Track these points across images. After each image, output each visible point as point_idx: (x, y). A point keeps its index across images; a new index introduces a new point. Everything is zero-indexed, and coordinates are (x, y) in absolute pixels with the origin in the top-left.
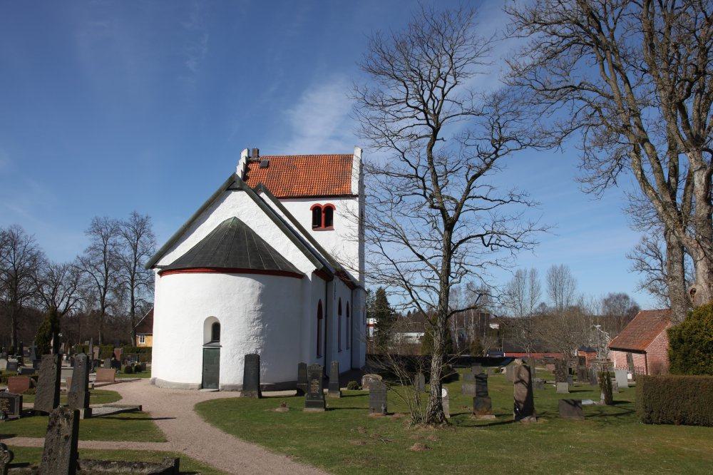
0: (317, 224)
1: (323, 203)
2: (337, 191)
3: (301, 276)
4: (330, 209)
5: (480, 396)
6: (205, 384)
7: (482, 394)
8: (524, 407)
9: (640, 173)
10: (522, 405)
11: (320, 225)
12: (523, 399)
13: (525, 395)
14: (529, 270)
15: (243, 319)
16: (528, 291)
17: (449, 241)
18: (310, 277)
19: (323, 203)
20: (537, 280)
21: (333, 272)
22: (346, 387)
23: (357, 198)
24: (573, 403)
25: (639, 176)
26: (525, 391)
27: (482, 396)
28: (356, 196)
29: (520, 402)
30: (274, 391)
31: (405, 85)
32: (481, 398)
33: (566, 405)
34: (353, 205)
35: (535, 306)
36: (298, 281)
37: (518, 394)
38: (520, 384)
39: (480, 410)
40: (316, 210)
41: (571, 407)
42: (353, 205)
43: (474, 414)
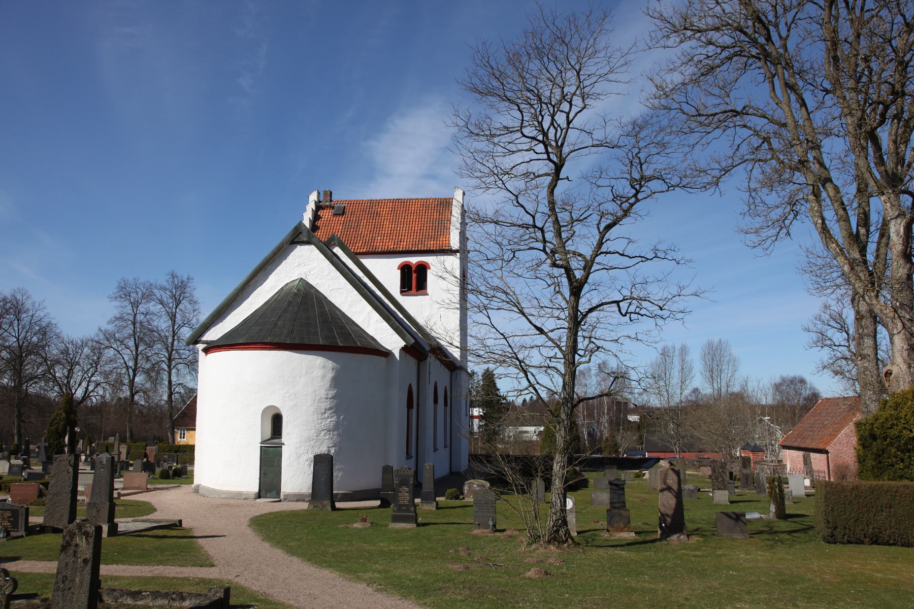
1: (414, 260)
2: (432, 245)
3: (387, 354)
4: (422, 269)
5: (615, 508)
8: (672, 521)
9: (820, 221)
10: (669, 520)
11: (410, 289)
12: (670, 512)
14: (678, 346)
18: (397, 355)
19: (414, 260)
20: (688, 358)
21: (427, 348)
23: (458, 254)
24: (734, 516)
25: (819, 226)
26: (673, 502)
27: (618, 508)
29: (668, 516)
32: (617, 510)
34: (453, 262)
35: (687, 392)
36: (382, 359)
37: (664, 505)
38: (666, 493)
40: (405, 270)
41: (732, 522)
42: (453, 262)
43: (608, 531)
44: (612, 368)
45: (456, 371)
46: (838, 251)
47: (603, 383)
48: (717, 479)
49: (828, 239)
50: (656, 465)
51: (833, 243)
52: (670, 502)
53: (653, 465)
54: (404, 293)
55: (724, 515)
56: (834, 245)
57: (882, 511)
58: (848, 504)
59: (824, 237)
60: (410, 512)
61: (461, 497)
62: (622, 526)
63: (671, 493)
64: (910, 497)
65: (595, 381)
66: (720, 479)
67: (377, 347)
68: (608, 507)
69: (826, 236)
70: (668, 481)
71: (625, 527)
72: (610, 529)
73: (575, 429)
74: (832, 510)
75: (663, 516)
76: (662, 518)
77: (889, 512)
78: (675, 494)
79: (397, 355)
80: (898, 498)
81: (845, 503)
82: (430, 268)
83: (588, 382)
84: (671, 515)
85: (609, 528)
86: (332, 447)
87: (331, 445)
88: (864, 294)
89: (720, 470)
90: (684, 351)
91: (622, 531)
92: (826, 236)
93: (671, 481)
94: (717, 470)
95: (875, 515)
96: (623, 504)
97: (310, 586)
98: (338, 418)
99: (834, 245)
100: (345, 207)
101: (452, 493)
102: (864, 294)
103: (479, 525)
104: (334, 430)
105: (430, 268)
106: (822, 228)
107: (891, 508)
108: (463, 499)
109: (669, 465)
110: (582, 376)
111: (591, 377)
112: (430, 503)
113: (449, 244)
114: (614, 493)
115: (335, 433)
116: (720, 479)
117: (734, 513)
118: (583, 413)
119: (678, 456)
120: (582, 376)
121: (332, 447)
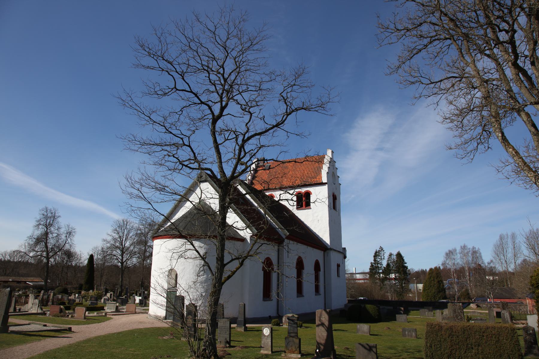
0: (300, 206)
1: (303, 190)
4: (308, 194)
5: (291, 337)
6: (168, 316)
7: (293, 335)
8: (324, 348)
9: (500, 135)
10: (322, 347)
11: (302, 206)
12: (323, 342)
13: (325, 337)
14: (509, 234)
15: (192, 271)
16: (510, 250)
17: (289, 200)
18: (249, 241)
19: (303, 190)
20: (517, 241)
21: (284, 237)
22: (270, 323)
23: (327, 185)
25: (500, 138)
26: (325, 334)
27: (293, 337)
28: (325, 184)
29: (321, 344)
30: (315, 320)
31: (236, 76)
33: (362, 349)
35: (519, 261)
36: (239, 243)
37: (319, 337)
38: (321, 327)
39: (290, 349)
41: (366, 352)
43: (285, 352)
44: (469, 249)
45: (327, 251)
46: (514, 153)
47: (464, 257)
48: (457, 317)
49: (507, 146)
50: (468, 306)
51: (510, 148)
52: (323, 334)
53: (466, 307)
54: (299, 209)
55: (361, 346)
56: (511, 149)
57: (472, 348)
58: (443, 342)
59: (504, 145)
60: (192, 332)
61: (281, 324)
62: (294, 349)
63: (324, 327)
64: (495, 338)
65: (459, 256)
66: (459, 317)
67: (243, 238)
68: (287, 336)
69: (505, 144)
70: (322, 319)
71: (295, 351)
72: (287, 351)
73: (441, 285)
74: (431, 346)
75: (318, 345)
76: (318, 346)
77: (478, 350)
78: (326, 328)
79: (249, 241)
80: (485, 338)
81: (441, 341)
82: (312, 194)
83: (455, 257)
84: (323, 344)
85: (286, 351)
86: (203, 292)
87: (203, 291)
88: (536, 182)
89: (459, 311)
90: (513, 236)
91: (294, 353)
92: (505, 144)
93: (324, 319)
94: (457, 311)
95: (466, 352)
96: (296, 334)
97: (486, 356)
98: (207, 276)
99: (511, 149)
100: (270, 165)
101: (274, 321)
102: (536, 182)
103: (221, 342)
104: (205, 283)
105: (312, 194)
106: (502, 139)
107: (479, 346)
108: (282, 326)
109: (476, 307)
110: (451, 254)
111: (456, 254)
112: (241, 327)
113: (321, 179)
114: (291, 326)
115: (205, 285)
116: (459, 317)
117: (367, 345)
118: (454, 275)
119: (492, 301)
120: (451, 254)
121: (203, 292)
